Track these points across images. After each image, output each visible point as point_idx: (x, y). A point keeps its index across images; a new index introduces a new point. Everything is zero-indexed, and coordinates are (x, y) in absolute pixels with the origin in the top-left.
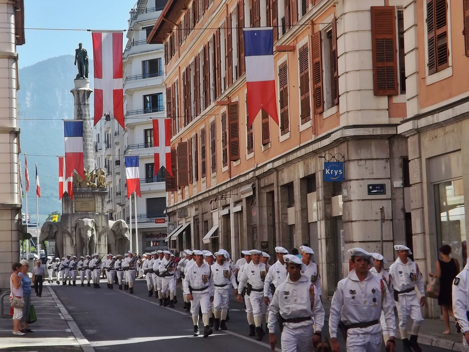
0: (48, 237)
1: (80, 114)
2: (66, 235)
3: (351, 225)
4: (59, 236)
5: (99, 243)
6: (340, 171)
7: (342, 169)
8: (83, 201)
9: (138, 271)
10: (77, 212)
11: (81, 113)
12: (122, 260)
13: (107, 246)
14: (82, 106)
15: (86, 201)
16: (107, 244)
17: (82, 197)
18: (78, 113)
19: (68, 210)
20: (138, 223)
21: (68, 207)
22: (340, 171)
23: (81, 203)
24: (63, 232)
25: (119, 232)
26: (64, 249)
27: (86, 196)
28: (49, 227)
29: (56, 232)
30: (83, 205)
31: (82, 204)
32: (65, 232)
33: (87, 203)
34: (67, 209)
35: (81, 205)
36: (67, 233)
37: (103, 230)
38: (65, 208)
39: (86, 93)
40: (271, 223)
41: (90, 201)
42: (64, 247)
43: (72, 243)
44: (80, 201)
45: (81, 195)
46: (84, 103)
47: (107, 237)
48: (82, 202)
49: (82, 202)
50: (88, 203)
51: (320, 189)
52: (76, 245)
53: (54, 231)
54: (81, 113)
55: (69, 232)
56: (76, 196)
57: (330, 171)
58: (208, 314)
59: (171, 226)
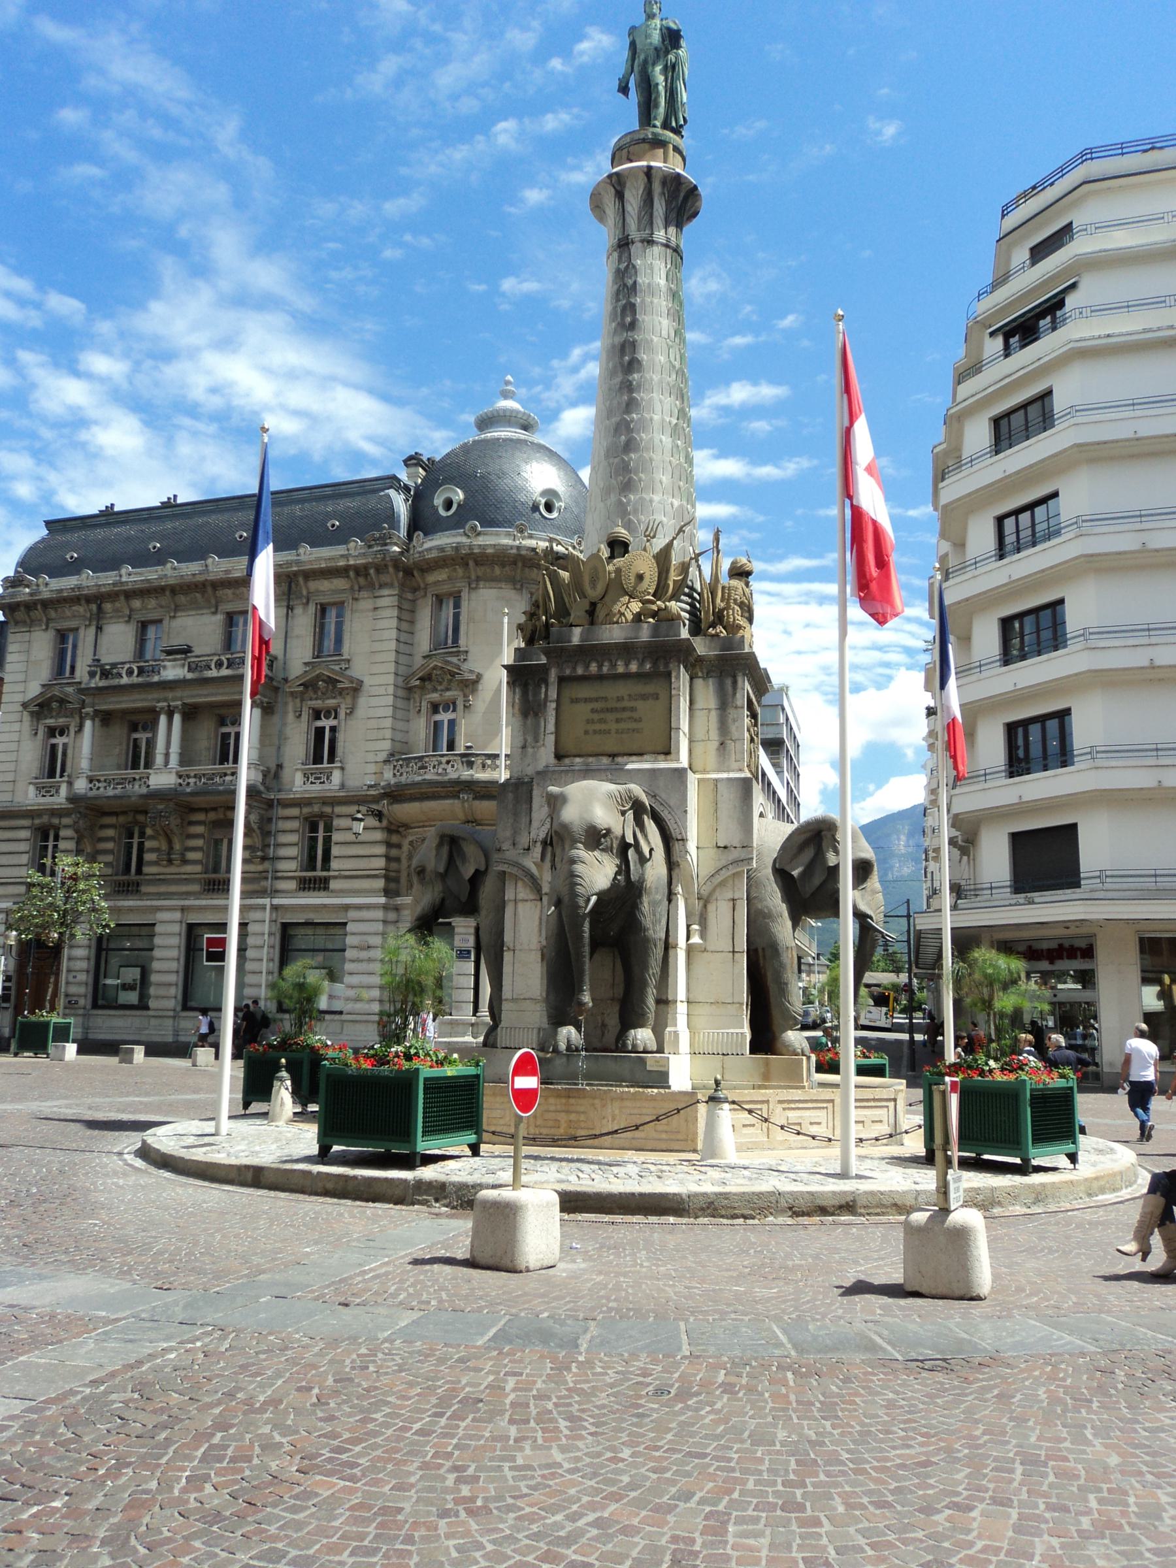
1: (625, 285)
8: (605, 699)
9: (678, 246)
10: (567, 761)
11: (630, 282)
12: (799, 1499)
14: (635, 249)
17: (600, 678)
18: (616, 287)
20: (260, 986)
23: (593, 711)
25: (817, 881)
27: (621, 669)
28: (445, 850)
30: (602, 721)
31: (596, 716)
33: (624, 709)
34: (530, 750)
35: (588, 721)
39: (657, 187)
40: (677, 847)
41: (644, 697)
44: (586, 700)
45: (593, 668)
46: (645, 234)
50: (633, 709)
53: (468, 871)
54: (630, 282)
56: (568, 672)
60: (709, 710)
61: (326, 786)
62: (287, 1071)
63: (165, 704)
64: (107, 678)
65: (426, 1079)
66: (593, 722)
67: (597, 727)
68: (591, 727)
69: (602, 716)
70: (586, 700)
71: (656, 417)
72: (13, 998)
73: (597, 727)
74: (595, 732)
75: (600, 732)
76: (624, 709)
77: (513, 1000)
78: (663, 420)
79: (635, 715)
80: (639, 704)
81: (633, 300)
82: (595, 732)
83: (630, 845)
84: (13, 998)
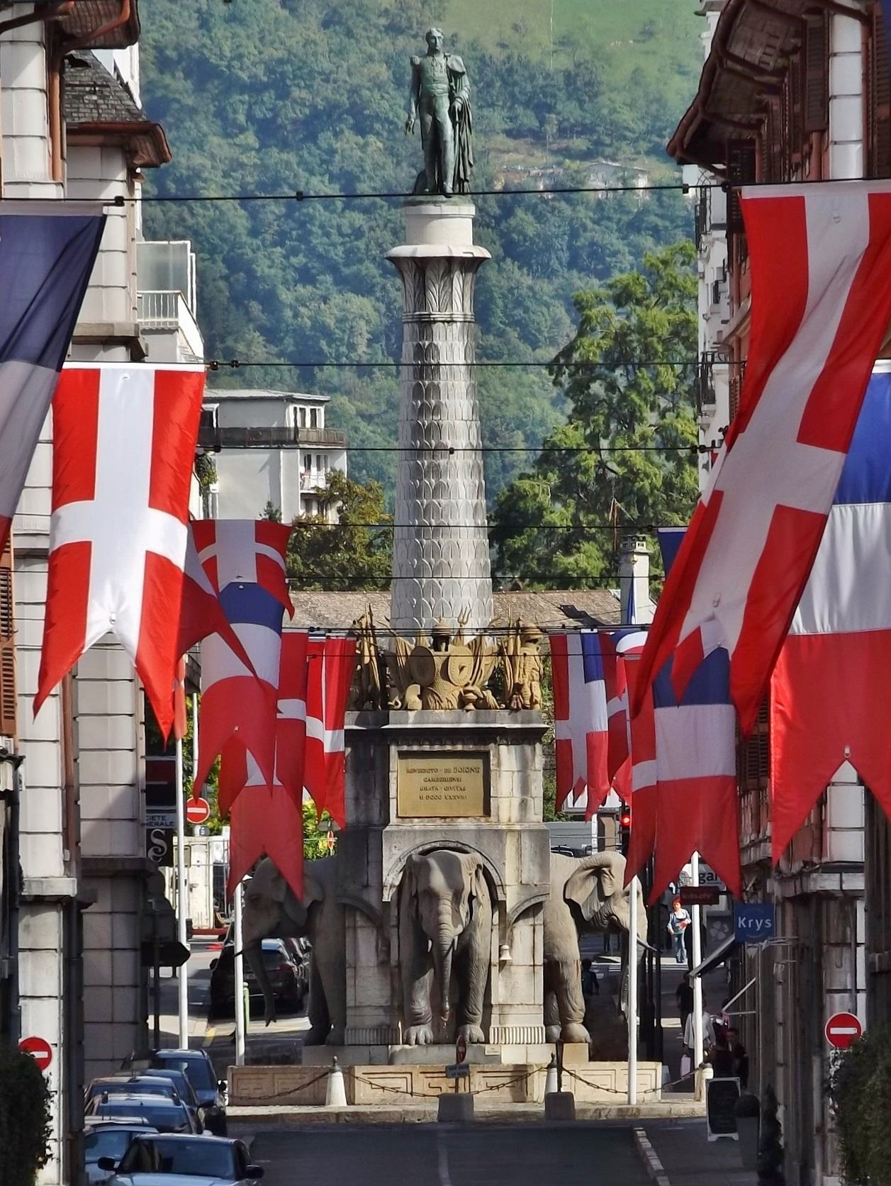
0: (279, 924)
2: (360, 921)
3: (831, 997)
4: (326, 921)
5: (506, 957)
6: (767, 921)
7: (771, 918)
13: (540, 971)
15: (447, 771)
16: (540, 960)
19: (368, 809)
21: (368, 792)
22: (767, 921)
24: (345, 906)
26: (349, 982)
29: (315, 903)
31: (429, 785)
32: (205, 135)
34: (363, 802)
36: (362, 911)
37: (523, 898)
38: (357, 799)
42: (349, 973)
43: (382, 957)
44: (422, 771)
47: (540, 931)
48: (430, 776)
49: (430, 776)
51: (56, 1098)
52: (399, 966)
55: (370, 907)
57: (746, 922)
58: (134, 913)
59: (717, 925)
60: (513, 772)
61: (178, 1051)
62: (183, 72)
63: (406, 327)
64: (560, 319)
65: (96, 372)
66: (426, 789)
67: (430, 793)
68: (425, 793)
69: (434, 784)
70: (422, 771)
71: (460, 502)
72: (302, 406)
73: (430, 793)
74: (428, 797)
75: (432, 798)
76: (452, 779)
77: (356, 1007)
78: (467, 503)
79: (461, 784)
80: (464, 776)
81: (436, 382)
82: (428, 797)
83: (474, 897)
84: (302, 406)
